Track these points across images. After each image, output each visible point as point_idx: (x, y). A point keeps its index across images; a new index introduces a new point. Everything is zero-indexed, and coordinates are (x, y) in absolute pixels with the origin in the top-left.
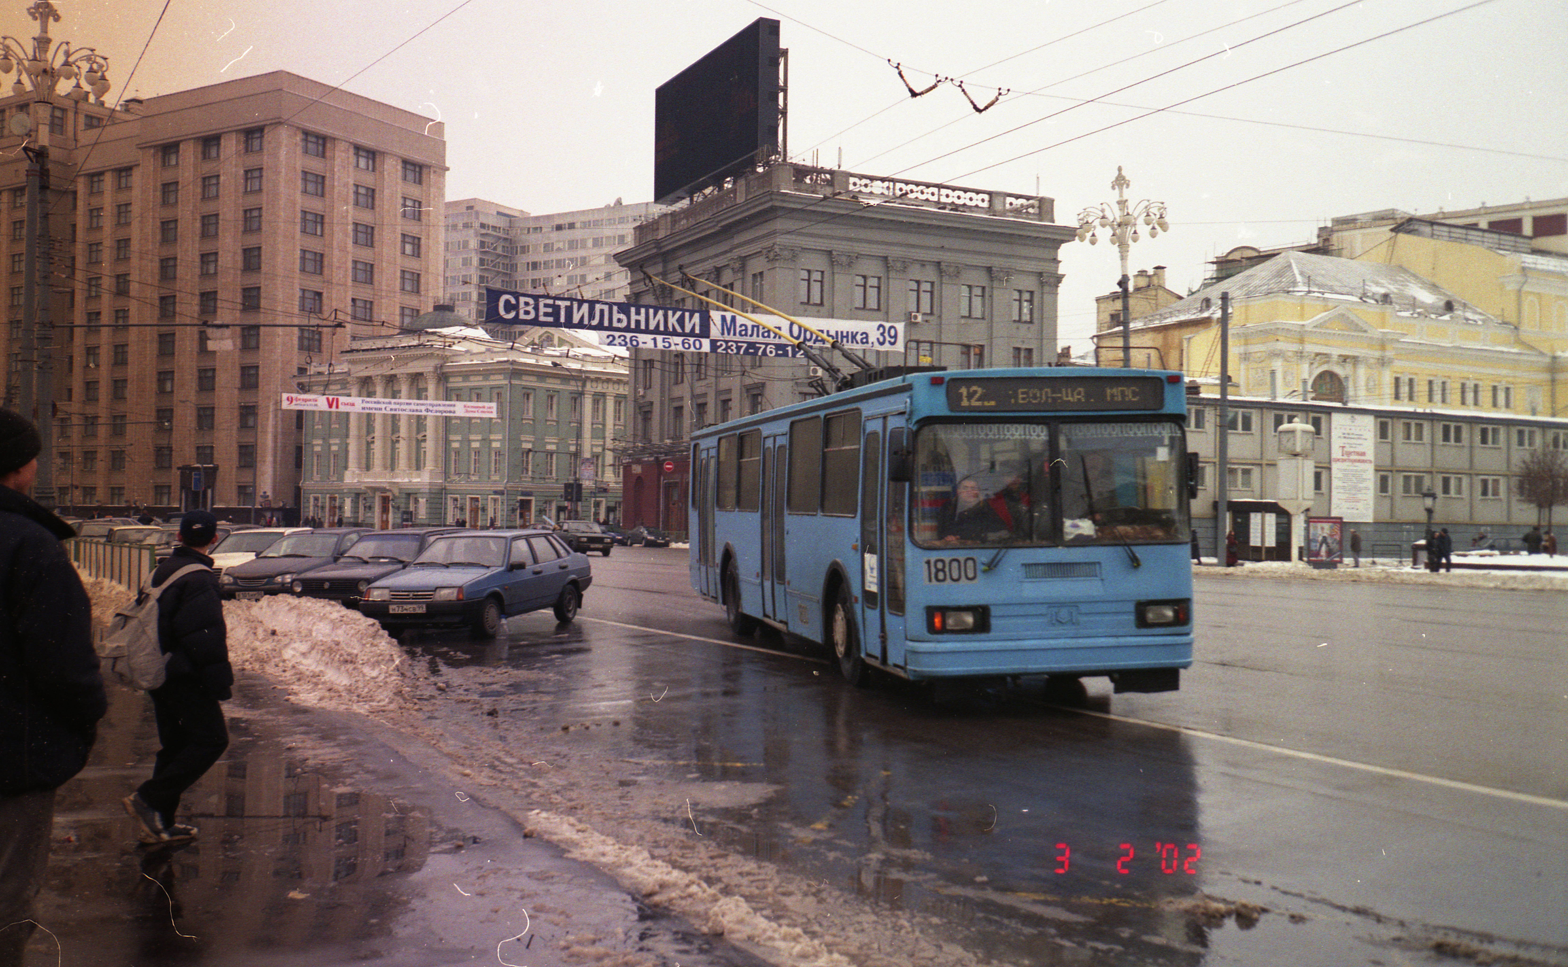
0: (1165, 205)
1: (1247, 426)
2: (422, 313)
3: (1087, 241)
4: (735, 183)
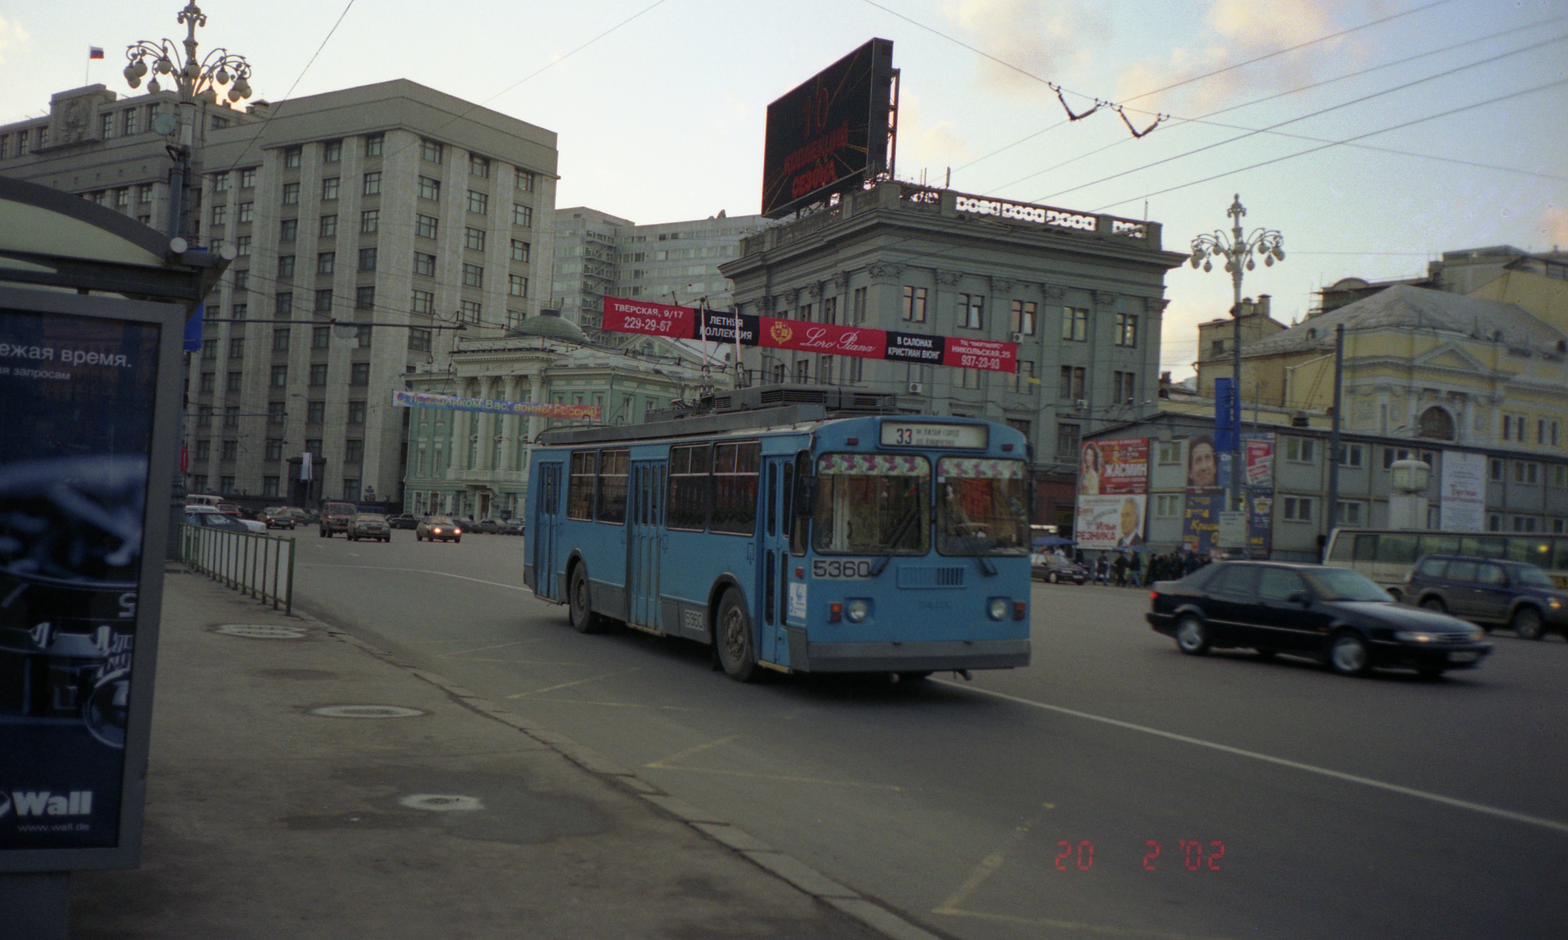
0: (1282, 234)
1: (1356, 459)
2: (528, 316)
3: (1201, 268)
4: (841, 199)
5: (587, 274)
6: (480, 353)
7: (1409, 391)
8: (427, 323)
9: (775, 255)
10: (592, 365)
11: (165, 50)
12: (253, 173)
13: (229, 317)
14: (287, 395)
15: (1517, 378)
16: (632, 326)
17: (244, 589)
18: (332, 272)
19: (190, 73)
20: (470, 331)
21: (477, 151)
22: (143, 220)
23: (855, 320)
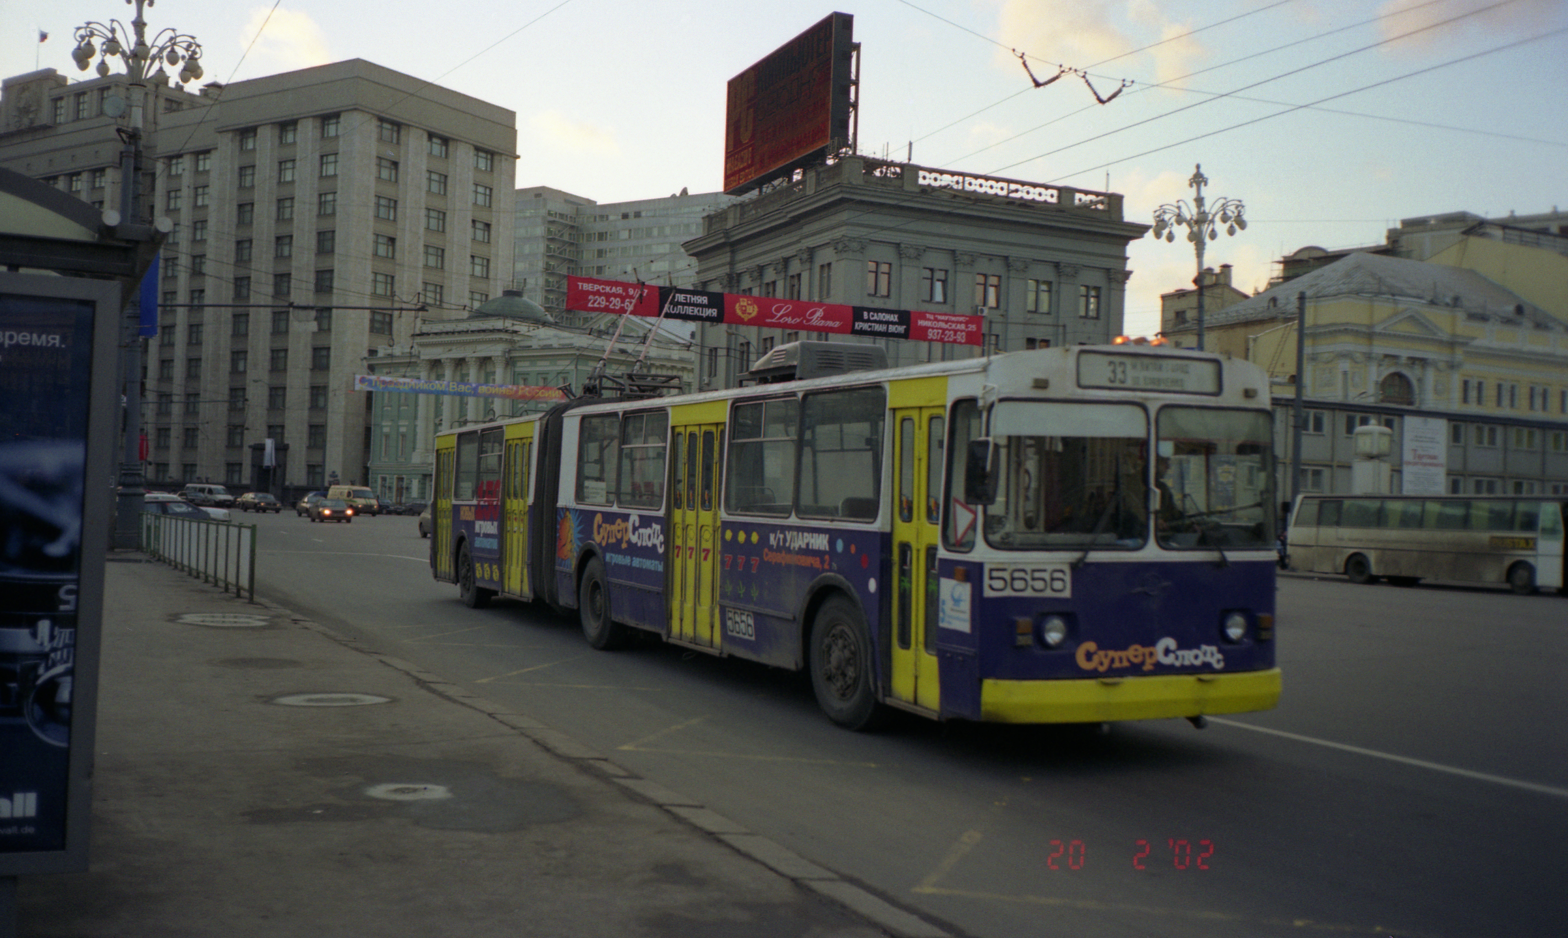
0: (1244, 203)
1: (1318, 426)
2: (491, 298)
3: (1164, 238)
4: (804, 174)
5: (550, 254)
6: (443, 336)
7: (1369, 357)
8: (388, 304)
9: (737, 232)
10: (555, 345)
11: (113, 31)
12: (208, 156)
13: (187, 302)
14: (248, 381)
15: (1476, 343)
16: (596, 305)
17: (207, 577)
18: (290, 256)
19: (139, 54)
20: (432, 312)
21: (436, 131)
22: (97, 206)
23: (821, 296)
